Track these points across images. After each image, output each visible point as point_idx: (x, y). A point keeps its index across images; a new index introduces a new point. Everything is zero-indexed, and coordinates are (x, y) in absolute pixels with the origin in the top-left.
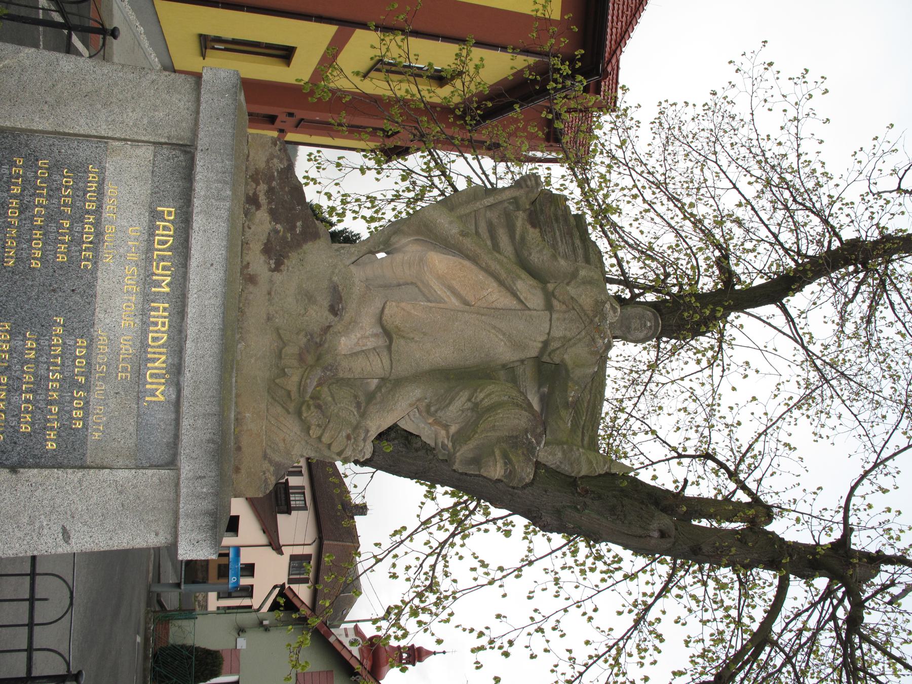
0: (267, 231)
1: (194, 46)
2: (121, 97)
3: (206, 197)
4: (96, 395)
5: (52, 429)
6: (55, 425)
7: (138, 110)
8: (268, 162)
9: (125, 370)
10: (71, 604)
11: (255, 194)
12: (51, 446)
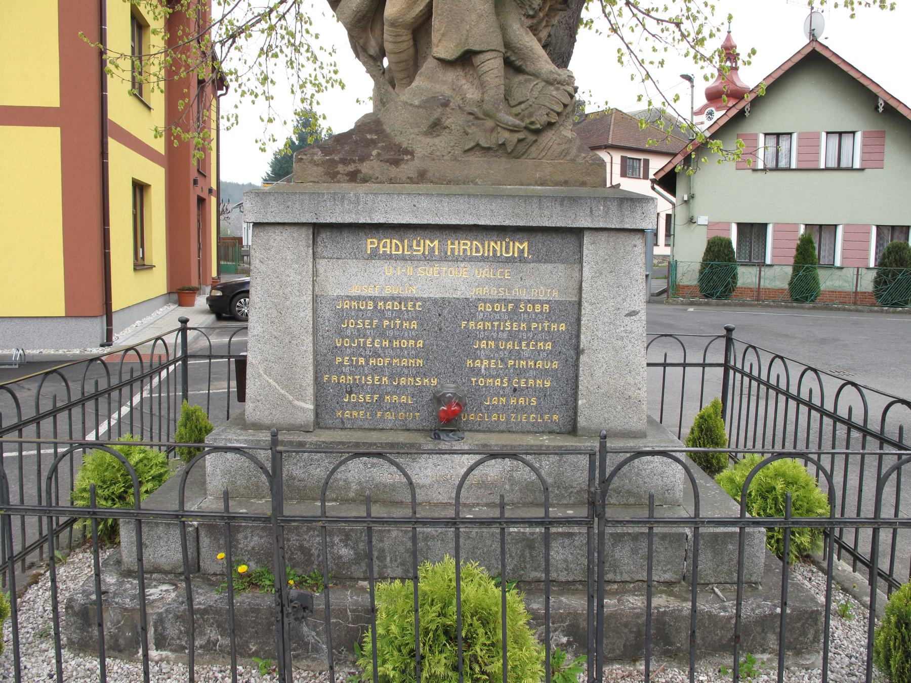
0: (379, 163)
1: (144, 276)
2: (278, 287)
3: (357, 213)
4: (524, 296)
5: (549, 327)
6: (546, 324)
7: (287, 272)
8: (317, 165)
9: (502, 273)
10: (671, 336)
11: (347, 175)
12: (563, 327)
